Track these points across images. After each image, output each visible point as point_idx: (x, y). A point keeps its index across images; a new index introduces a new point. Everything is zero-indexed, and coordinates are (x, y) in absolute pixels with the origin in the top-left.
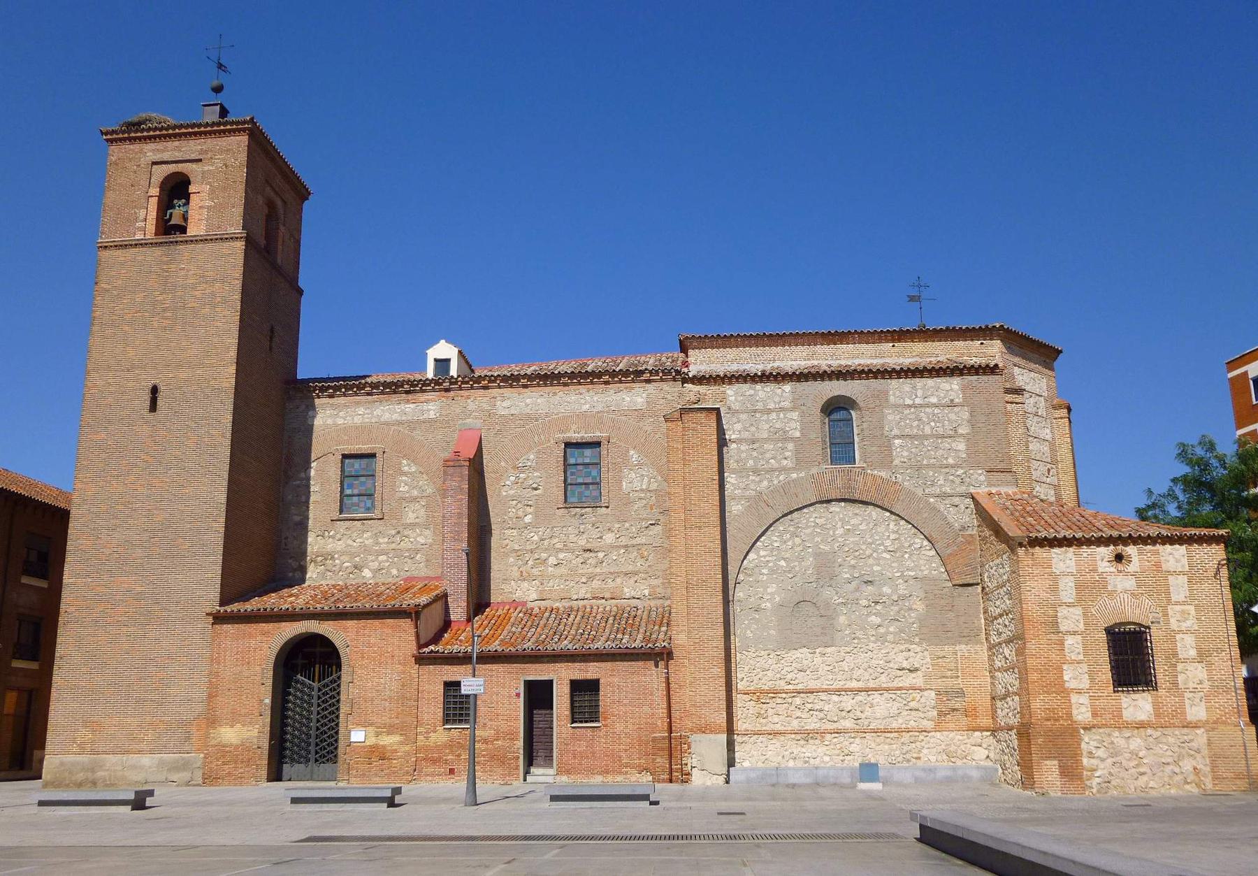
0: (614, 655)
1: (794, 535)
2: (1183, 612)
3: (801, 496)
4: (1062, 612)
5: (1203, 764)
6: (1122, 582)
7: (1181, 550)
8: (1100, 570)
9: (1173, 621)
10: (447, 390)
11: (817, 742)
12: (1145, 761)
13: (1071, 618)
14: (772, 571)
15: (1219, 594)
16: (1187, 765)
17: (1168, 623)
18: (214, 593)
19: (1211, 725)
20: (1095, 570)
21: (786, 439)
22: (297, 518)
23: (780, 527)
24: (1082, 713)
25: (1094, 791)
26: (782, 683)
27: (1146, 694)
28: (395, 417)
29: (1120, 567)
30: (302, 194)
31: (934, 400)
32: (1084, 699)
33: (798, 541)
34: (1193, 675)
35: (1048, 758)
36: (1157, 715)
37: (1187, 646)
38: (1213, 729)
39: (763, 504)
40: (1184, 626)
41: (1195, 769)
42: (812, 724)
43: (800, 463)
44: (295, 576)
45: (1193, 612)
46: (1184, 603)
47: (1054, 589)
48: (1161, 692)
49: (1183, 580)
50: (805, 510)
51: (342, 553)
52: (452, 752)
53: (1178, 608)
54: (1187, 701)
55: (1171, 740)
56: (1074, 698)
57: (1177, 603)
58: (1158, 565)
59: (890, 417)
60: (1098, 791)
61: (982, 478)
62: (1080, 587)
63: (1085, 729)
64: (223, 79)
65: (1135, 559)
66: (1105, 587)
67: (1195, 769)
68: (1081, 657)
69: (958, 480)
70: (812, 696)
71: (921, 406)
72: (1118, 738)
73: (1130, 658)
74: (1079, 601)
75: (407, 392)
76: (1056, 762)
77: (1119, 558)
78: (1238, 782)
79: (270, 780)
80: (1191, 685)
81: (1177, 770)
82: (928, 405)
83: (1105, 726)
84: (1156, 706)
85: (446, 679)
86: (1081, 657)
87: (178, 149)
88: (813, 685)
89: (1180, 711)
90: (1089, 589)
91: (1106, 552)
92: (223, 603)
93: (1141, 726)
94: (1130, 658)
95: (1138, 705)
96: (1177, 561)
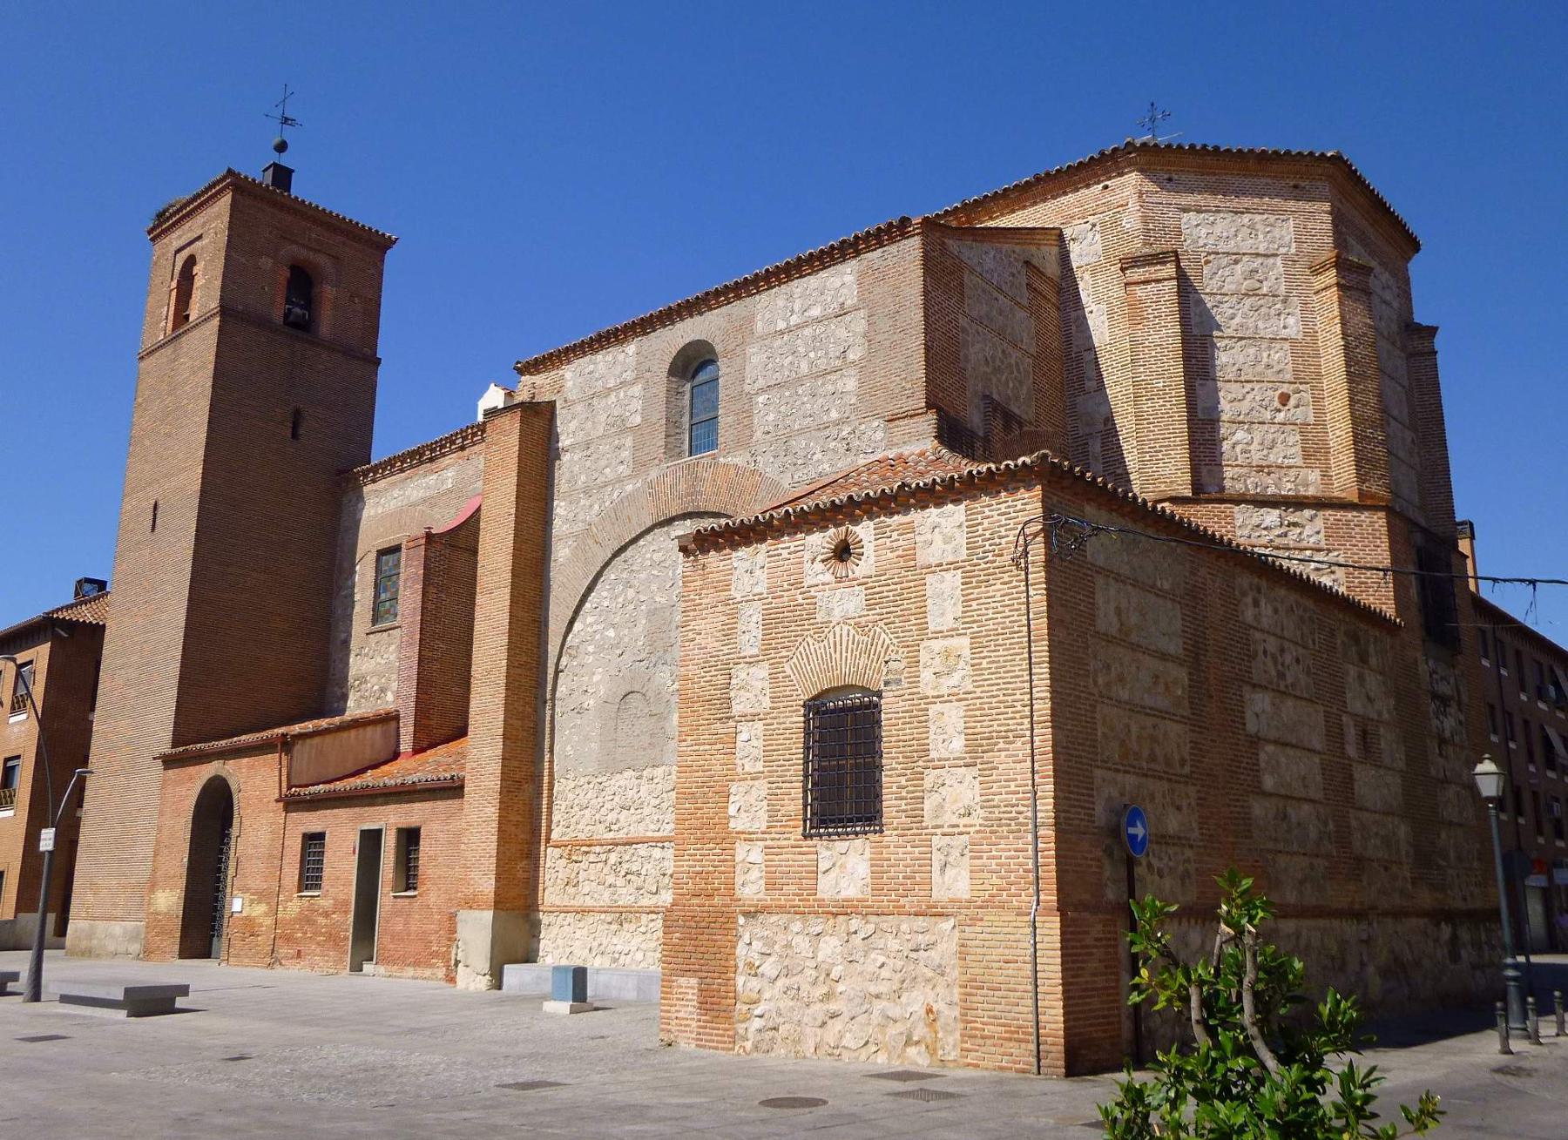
0: (400, 793)
1: (628, 584)
2: (947, 654)
3: (634, 520)
4: (741, 674)
5: (945, 1000)
6: (842, 602)
7: (954, 514)
8: (808, 581)
9: (926, 675)
10: (462, 448)
11: (633, 927)
12: (840, 988)
13: (752, 688)
14: (600, 648)
15: (1019, 603)
16: (915, 1002)
17: (915, 680)
18: (167, 735)
19: (969, 912)
20: (797, 584)
21: (624, 430)
22: (343, 636)
23: (610, 575)
24: (751, 888)
25: (748, 1045)
26: (601, 827)
27: (859, 842)
28: (421, 494)
29: (841, 569)
30: (1412, 245)
31: (816, 312)
32: (756, 855)
33: (631, 593)
34: (955, 795)
35: (685, 972)
36: (877, 889)
37: (948, 732)
38: (975, 920)
39: (590, 542)
40: (946, 685)
41: (929, 1011)
42: (626, 897)
43: (639, 465)
44: (342, 712)
45: (966, 652)
46: (953, 633)
47: (728, 633)
48: (890, 836)
49: (954, 579)
50: (641, 542)
51: (373, 674)
52: (301, 929)
53: (937, 645)
54: (936, 856)
55: (893, 944)
56: (741, 850)
57: (938, 635)
58: (910, 555)
59: (755, 360)
60: (756, 1048)
61: (879, 435)
62: (771, 622)
63: (746, 914)
64: (289, 134)
65: (869, 549)
66: (811, 616)
67: (929, 1011)
68: (759, 766)
69: (841, 447)
70: (630, 850)
71: (798, 327)
72: (798, 935)
73: (845, 761)
74: (769, 649)
75: (431, 460)
76: (694, 981)
77: (843, 552)
78: (1013, 1048)
79: (184, 954)
80: (949, 818)
81: (895, 1012)
82: (805, 324)
83: (782, 909)
84: (878, 868)
85: (304, 829)
86: (759, 766)
87: (190, 229)
88: (637, 831)
89: (919, 877)
90: (788, 620)
91: (820, 541)
92: (175, 744)
93: (844, 909)
94: (845, 761)
95: (847, 864)
96: (948, 540)
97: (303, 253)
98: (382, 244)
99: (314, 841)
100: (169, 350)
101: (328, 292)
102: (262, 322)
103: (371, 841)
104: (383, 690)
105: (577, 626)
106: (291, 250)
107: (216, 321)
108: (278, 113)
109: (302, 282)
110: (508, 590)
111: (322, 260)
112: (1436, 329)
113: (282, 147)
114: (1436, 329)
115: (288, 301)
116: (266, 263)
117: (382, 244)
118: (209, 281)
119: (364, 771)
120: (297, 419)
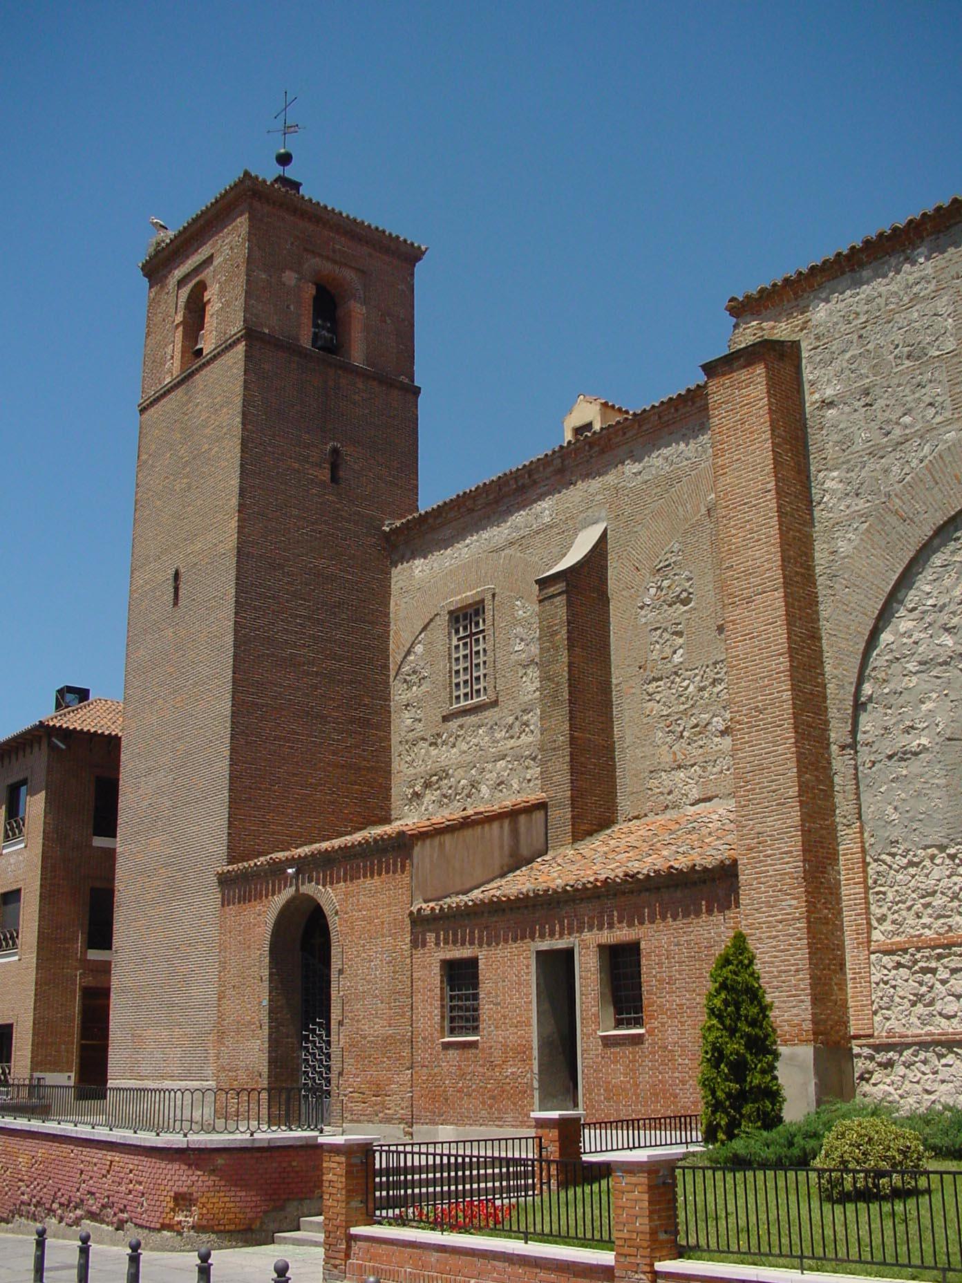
18: (221, 849)
39: (893, 520)
97: (327, 267)
98: (410, 256)
99: (461, 976)
100: (179, 392)
101: (358, 312)
102: (292, 348)
103: (557, 971)
104: (474, 785)
105: (886, 637)
106: (313, 263)
107: (241, 347)
108: (279, 124)
109: (327, 304)
110: (779, 594)
111: (349, 275)
112: (19, 890)
113: (284, 159)
114: (19, 890)
115: (315, 325)
116: (290, 278)
117: (410, 256)
118: (227, 304)
119: (471, 890)
120: (335, 461)
